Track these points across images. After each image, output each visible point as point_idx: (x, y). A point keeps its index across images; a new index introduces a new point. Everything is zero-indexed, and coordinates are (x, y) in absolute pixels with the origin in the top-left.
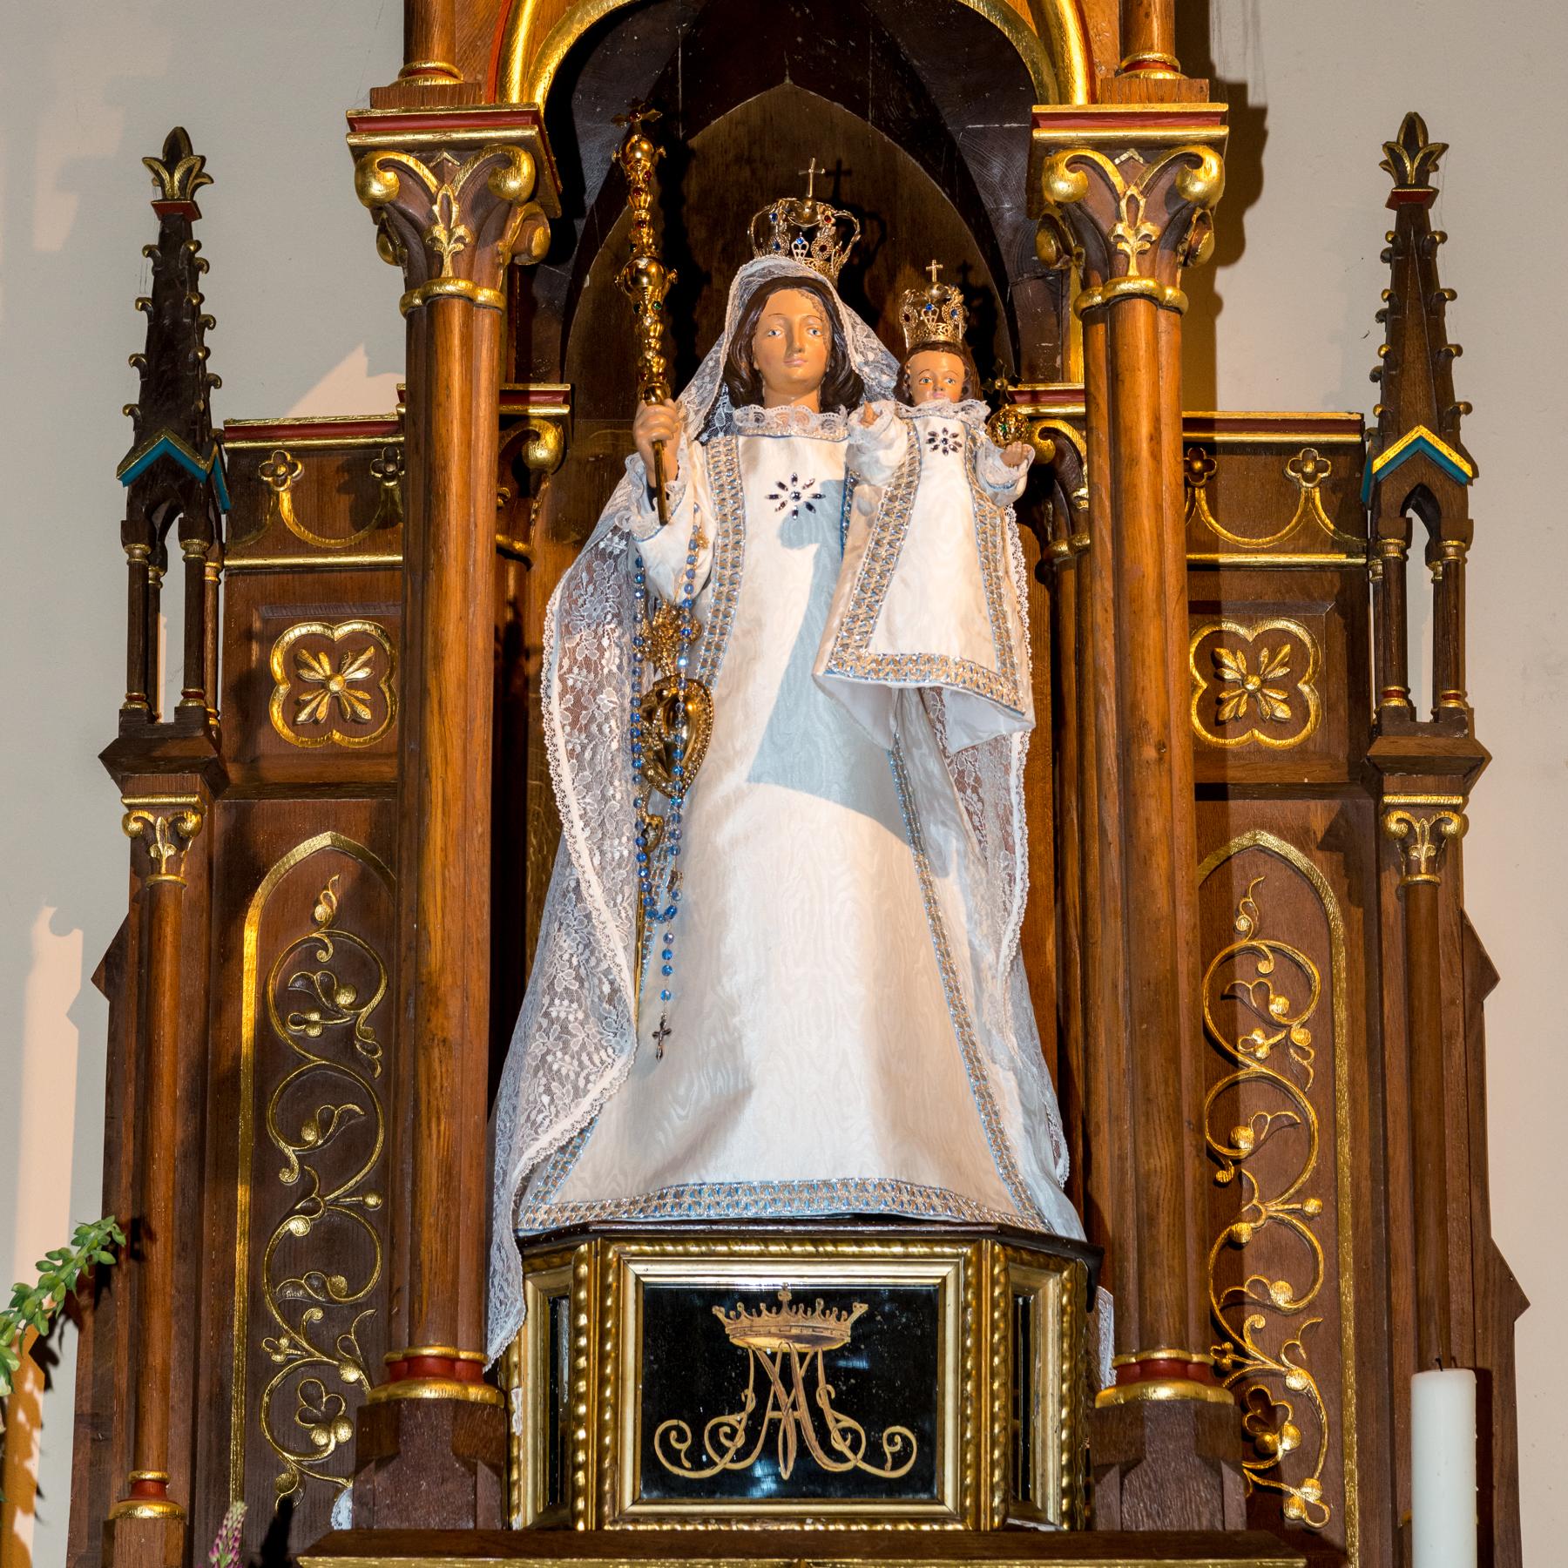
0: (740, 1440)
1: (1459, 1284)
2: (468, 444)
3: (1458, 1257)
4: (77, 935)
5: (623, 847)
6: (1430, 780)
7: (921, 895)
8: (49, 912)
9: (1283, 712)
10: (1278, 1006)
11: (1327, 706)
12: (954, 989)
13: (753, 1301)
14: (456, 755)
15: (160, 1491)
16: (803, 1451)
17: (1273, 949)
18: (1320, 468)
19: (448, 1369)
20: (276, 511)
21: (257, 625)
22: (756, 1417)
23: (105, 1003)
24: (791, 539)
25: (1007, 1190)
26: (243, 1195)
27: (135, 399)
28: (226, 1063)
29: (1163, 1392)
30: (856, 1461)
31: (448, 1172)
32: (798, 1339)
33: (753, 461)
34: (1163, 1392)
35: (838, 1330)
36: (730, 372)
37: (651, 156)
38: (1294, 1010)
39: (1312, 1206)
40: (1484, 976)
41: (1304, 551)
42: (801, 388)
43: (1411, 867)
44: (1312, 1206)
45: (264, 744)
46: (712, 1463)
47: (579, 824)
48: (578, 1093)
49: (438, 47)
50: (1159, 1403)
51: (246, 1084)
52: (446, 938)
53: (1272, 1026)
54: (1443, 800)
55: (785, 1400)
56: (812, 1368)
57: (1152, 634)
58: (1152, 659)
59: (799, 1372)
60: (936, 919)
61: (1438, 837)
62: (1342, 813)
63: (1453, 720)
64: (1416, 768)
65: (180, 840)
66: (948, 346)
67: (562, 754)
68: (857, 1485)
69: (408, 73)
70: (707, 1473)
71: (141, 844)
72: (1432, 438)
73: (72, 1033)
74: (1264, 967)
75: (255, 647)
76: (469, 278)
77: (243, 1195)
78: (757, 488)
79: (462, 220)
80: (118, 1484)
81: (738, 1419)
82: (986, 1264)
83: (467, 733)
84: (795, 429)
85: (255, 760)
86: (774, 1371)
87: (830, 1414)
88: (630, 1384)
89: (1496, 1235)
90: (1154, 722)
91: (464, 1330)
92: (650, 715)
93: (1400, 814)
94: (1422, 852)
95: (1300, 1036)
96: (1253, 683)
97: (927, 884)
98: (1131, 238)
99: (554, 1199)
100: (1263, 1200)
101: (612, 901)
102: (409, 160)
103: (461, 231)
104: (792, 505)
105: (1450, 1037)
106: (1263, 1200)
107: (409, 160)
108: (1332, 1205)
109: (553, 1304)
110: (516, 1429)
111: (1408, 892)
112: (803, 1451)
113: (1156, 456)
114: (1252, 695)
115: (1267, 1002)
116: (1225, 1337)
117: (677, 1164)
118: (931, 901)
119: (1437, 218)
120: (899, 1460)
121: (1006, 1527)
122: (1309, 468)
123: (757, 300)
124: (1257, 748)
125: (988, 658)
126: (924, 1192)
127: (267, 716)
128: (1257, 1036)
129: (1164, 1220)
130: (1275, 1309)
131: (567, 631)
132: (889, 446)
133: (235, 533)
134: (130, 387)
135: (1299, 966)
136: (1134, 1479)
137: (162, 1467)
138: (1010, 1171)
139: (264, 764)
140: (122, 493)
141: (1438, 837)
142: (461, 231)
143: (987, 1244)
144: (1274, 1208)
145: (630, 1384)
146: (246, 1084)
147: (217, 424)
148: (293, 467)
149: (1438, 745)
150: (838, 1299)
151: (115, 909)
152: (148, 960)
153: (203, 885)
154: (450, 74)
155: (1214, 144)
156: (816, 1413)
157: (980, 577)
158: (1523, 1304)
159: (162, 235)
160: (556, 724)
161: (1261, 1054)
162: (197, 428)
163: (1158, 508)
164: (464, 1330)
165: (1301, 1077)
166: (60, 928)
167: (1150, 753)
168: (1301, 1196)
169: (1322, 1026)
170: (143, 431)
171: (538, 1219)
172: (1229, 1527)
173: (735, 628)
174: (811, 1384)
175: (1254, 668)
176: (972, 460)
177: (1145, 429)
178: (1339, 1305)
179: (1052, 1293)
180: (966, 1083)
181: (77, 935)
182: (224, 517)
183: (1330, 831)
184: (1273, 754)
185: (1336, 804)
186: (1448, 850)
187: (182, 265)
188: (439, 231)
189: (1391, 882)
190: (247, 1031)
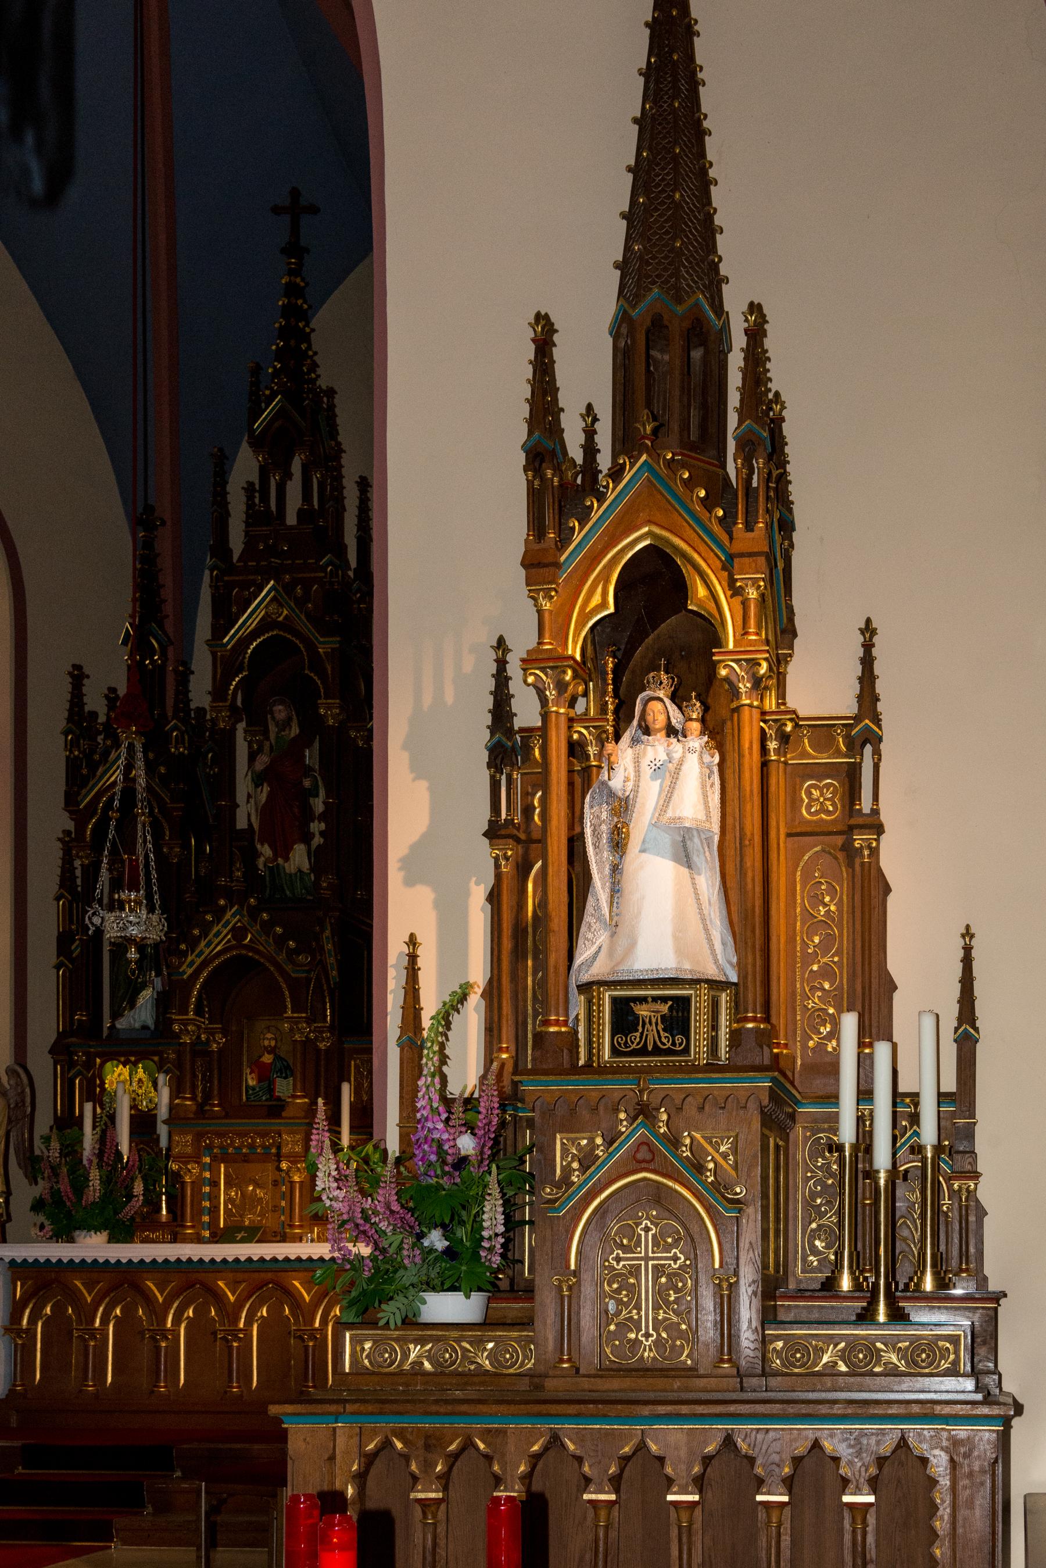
0: (638, 1040)
1: (875, 982)
2: (558, 757)
3: (874, 974)
4: (483, 885)
5: (607, 871)
6: (867, 831)
7: (690, 883)
8: (474, 879)
9: (831, 808)
10: (827, 899)
11: (843, 806)
12: (700, 909)
13: (643, 1000)
14: (555, 848)
15: (507, 1050)
16: (655, 1042)
17: (826, 882)
18: (842, 731)
19: (557, 1023)
20: (534, 755)
21: (530, 790)
22: (642, 1034)
23: (490, 906)
24: (653, 778)
25: (714, 967)
26: (530, 963)
27: (490, 724)
28: (524, 925)
29: (750, 1025)
30: (669, 1045)
31: (555, 967)
32: (653, 1012)
33: (645, 753)
34: (750, 1025)
35: (665, 1008)
36: (640, 726)
37: (612, 662)
38: (831, 901)
39: (836, 959)
40: (887, 890)
41: (837, 758)
42: (659, 730)
43: (863, 857)
44: (836, 959)
45: (532, 826)
46: (630, 1047)
47: (595, 865)
48: (593, 943)
49: (547, 635)
50: (748, 1028)
51: (530, 930)
52: (553, 902)
53: (825, 905)
54: (871, 837)
55: (650, 1029)
56: (657, 1019)
57: (748, 807)
58: (748, 815)
59: (654, 1020)
60: (695, 889)
61: (870, 847)
62: (847, 838)
63: (875, 812)
64: (863, 827)
65: (507, 859)
66: (696, 720)
67: (590, 844)
68: (670, 1052)
69: (539, 643)
70: (629, 1049)
71: (496, 859)
72: (871, 724)
73: (482, 915)
74: (823, 887)
75: (530, 797)
76: (557, 706)
77: (530, 963)
78: (645, 763)
79: (554, 689)
80: (495, 1048)
81: (638, 1034)
82: (702, 990)
83: (559, 841)
84: (657, 743)
85: (530, 833)
86: (647, 1021)
87: (662, 1033)
88: (607, 1025)
89: (889, 967)
90: (748, 833)
91: (561, 1011)
92: (613, 833)
93: (858, 842)
94: (866, 852)
95: (833, 908)
96: (822, 800)
97: (693, 879)
98: (744, 687)
99: (590, 973)
100: (821, 957)
101: (603, 888)
102: (537, 672)
103: (553, 692)
104: (654, 768)
105: (874, 908)
106: (821, 957)
107: (537, 672)
108: (841, 959)
109: (589, 1002)
110: (580, 1037)
111: (863, 864)
112: (655, 1042)
113: (751, 754)
114: (821, 803)
115: (824, 898)
116: (809, 999)
117: (618, 964)
118: (694, 884)
119: (875, 652)
120: (681, 1045)
121: (708, 1064)
122: (839, 731)
123: (645, 704)
124: (822, 820)
125: (702, 816)
126: (685, 970)
127: (533, 819)
128: (821, 908)
129: (750, 977)
130: (825, 990)
131: (592, 807)
132: (676, 752)
133: (523, 762)
134: (488, 719)
135: (834, 887)
136: (739, 1049)
137: (507, 1043)
138: (716, 961)
139: (532, 834)
140: (487, 753)
141: (870, 847)
142: (553, 692)
143: (702, 984)
144: (825, 960)
145: (607, 1025)
146: (530, 930)
147: (516, 728)
148: (539, 741)
149: (869, 821)
150: (664, 999)
151: (491, 881)
152: (499, 894)
153: (515, 872)
154: (552, 644)
155: (766, 659)
156: (658, 1032)
157: (700, 791)
158: (896, 988)
159: (497, 670)
160: (589, 835)
161: (822, 913)
162: (510, 732)
163: (751, 769)
164: (561, 1011)
165: (833, 920)
166: (477, 884)
167: (747, 843)
168: (833, 956)
169: (839, 905)
170: (492, 734)
171: (585, 978)
172: (765, 1063)
173: (637, 805)
174: (657, 1024)
175: (822, 794)
176: (701, 757)
177: (747, 745)
178: (843, 989)
179: (724, 997)
180: (703, 936)
181: (483, 885)
182: (519, 757)
183: (842, 846)
184: (826, 821)
185: (845, 837)
186: (875, 852)
187: (503, 680)
188: (548, 693)
189: (858, 861)
190: (530, 914)
